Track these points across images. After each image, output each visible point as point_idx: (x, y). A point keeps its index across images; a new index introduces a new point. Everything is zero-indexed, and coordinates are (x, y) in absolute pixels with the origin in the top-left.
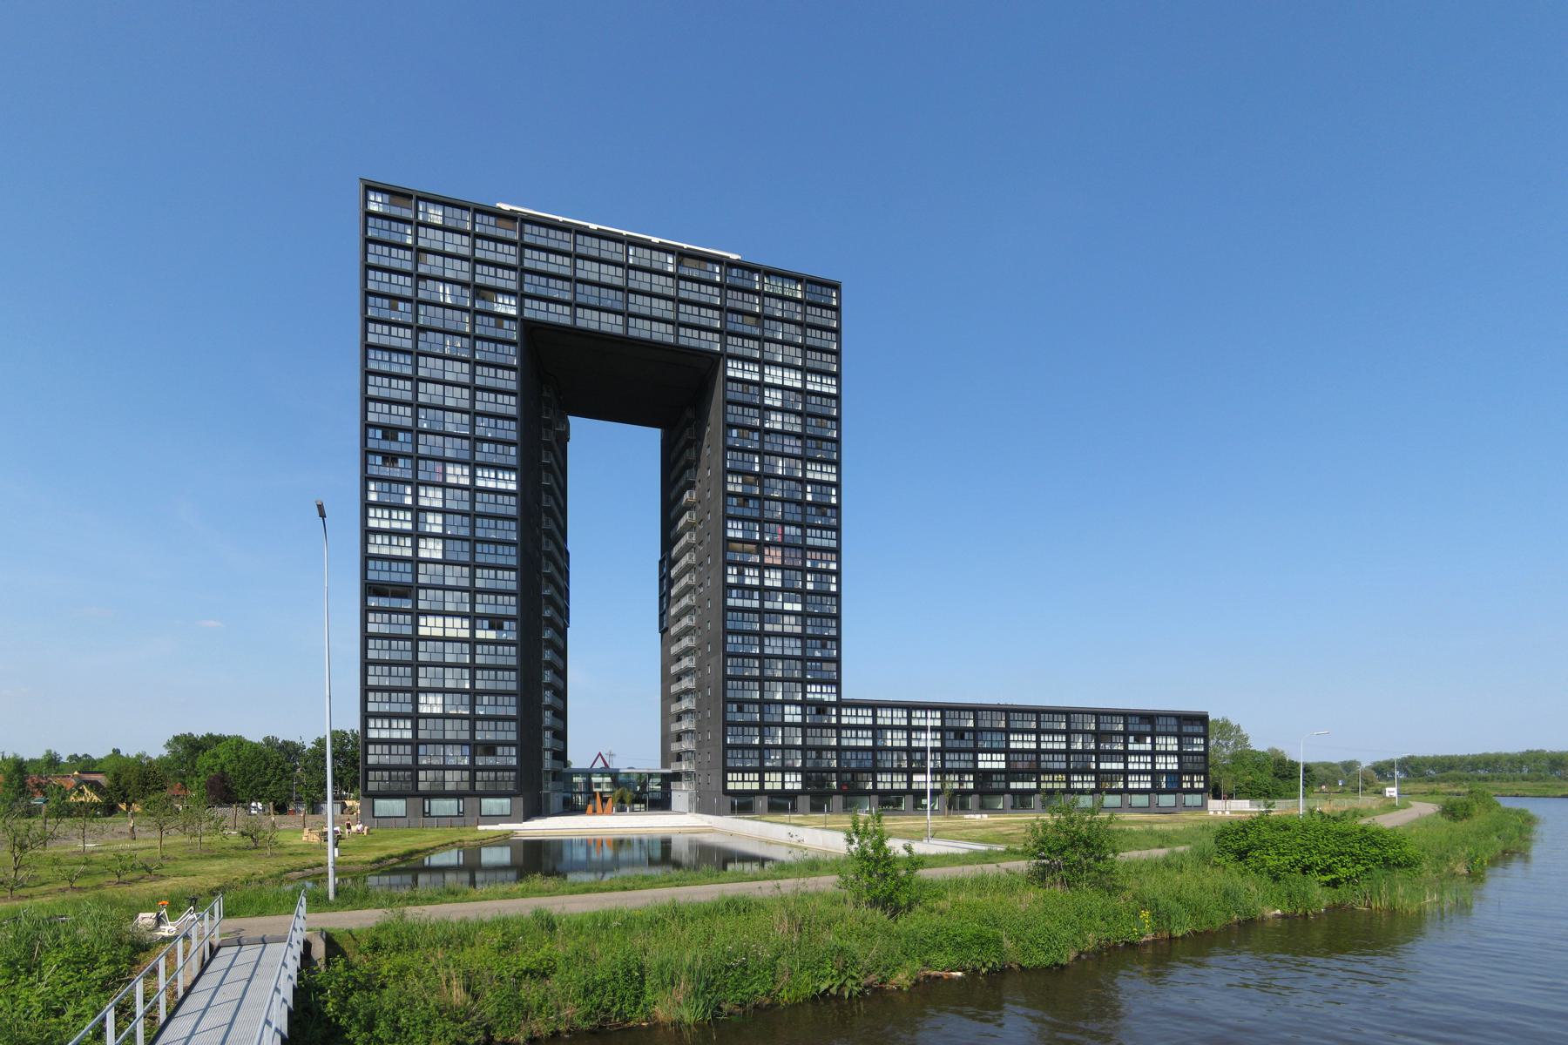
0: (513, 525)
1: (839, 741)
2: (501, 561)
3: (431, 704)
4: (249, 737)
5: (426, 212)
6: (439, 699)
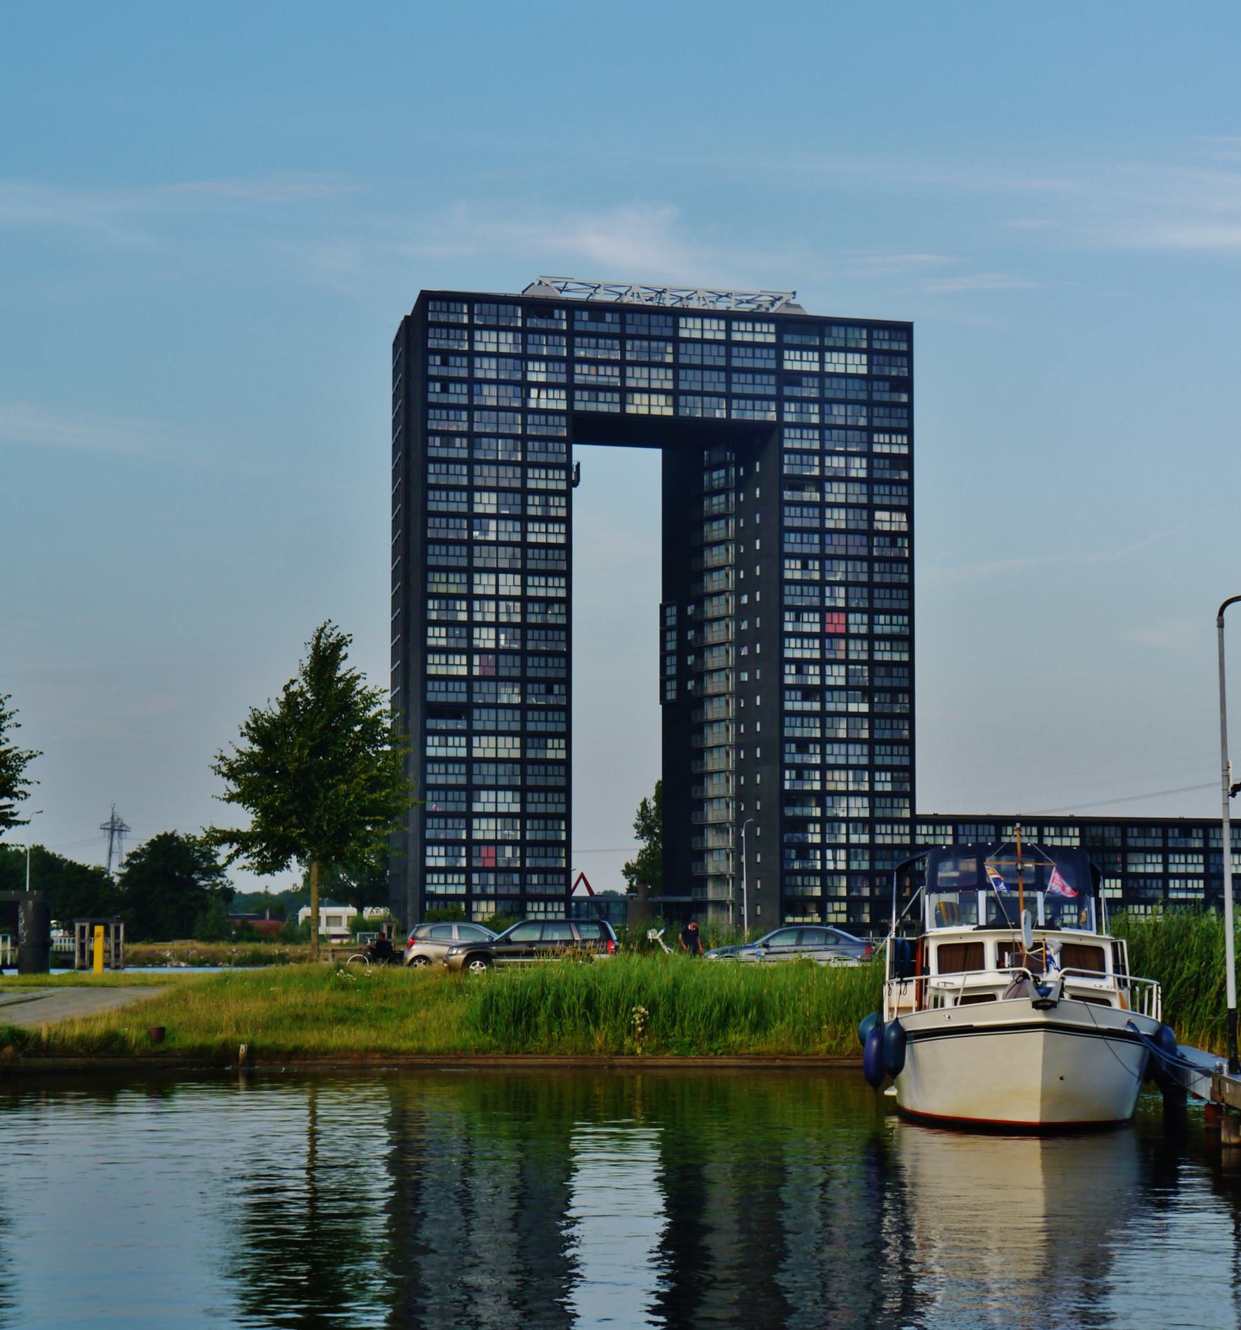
1: (469, 834)
3: (811, 624)
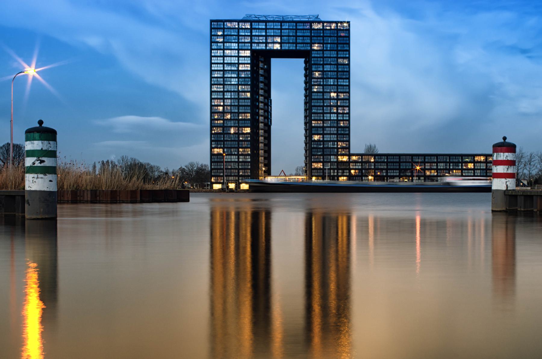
0: (249, 65)
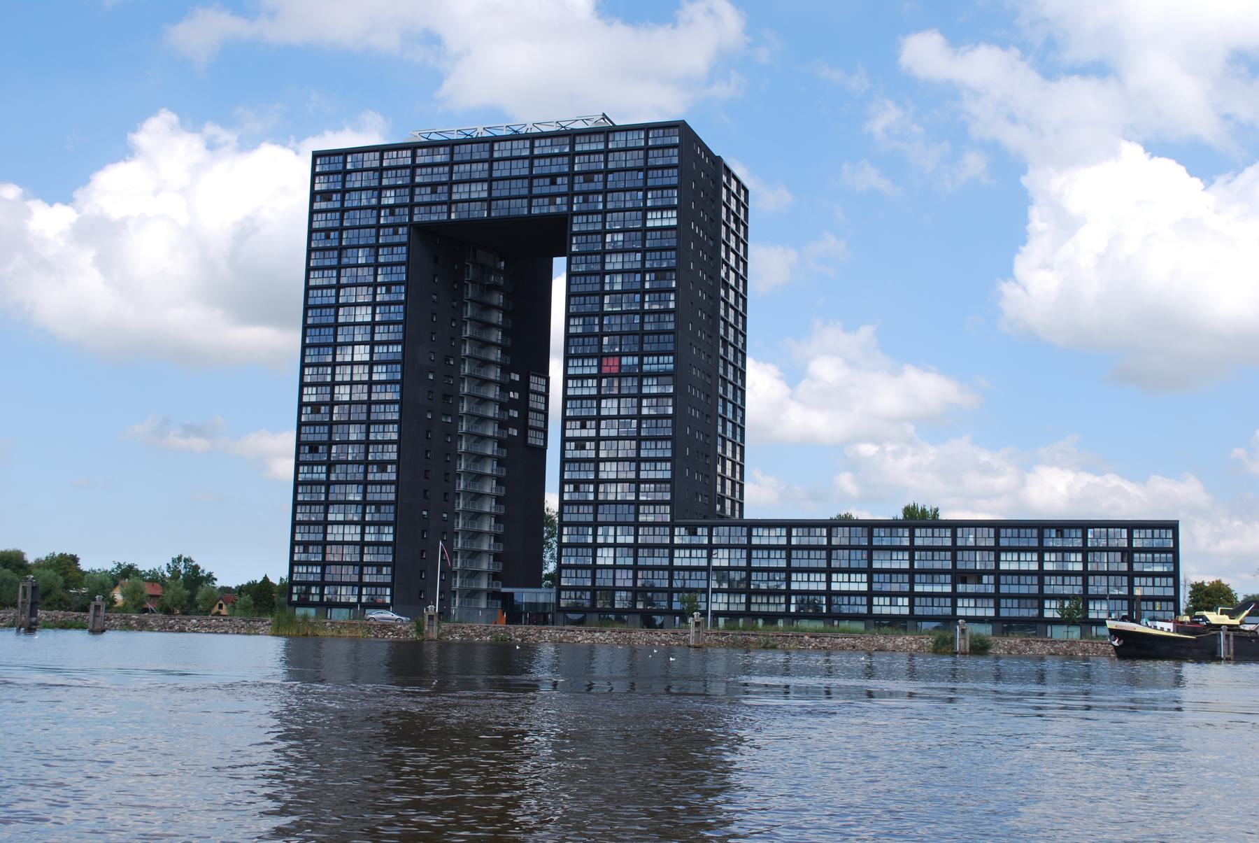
2: (813, 564)
4: (144, 566)
5: (605, 492)
6: (620, 258)
